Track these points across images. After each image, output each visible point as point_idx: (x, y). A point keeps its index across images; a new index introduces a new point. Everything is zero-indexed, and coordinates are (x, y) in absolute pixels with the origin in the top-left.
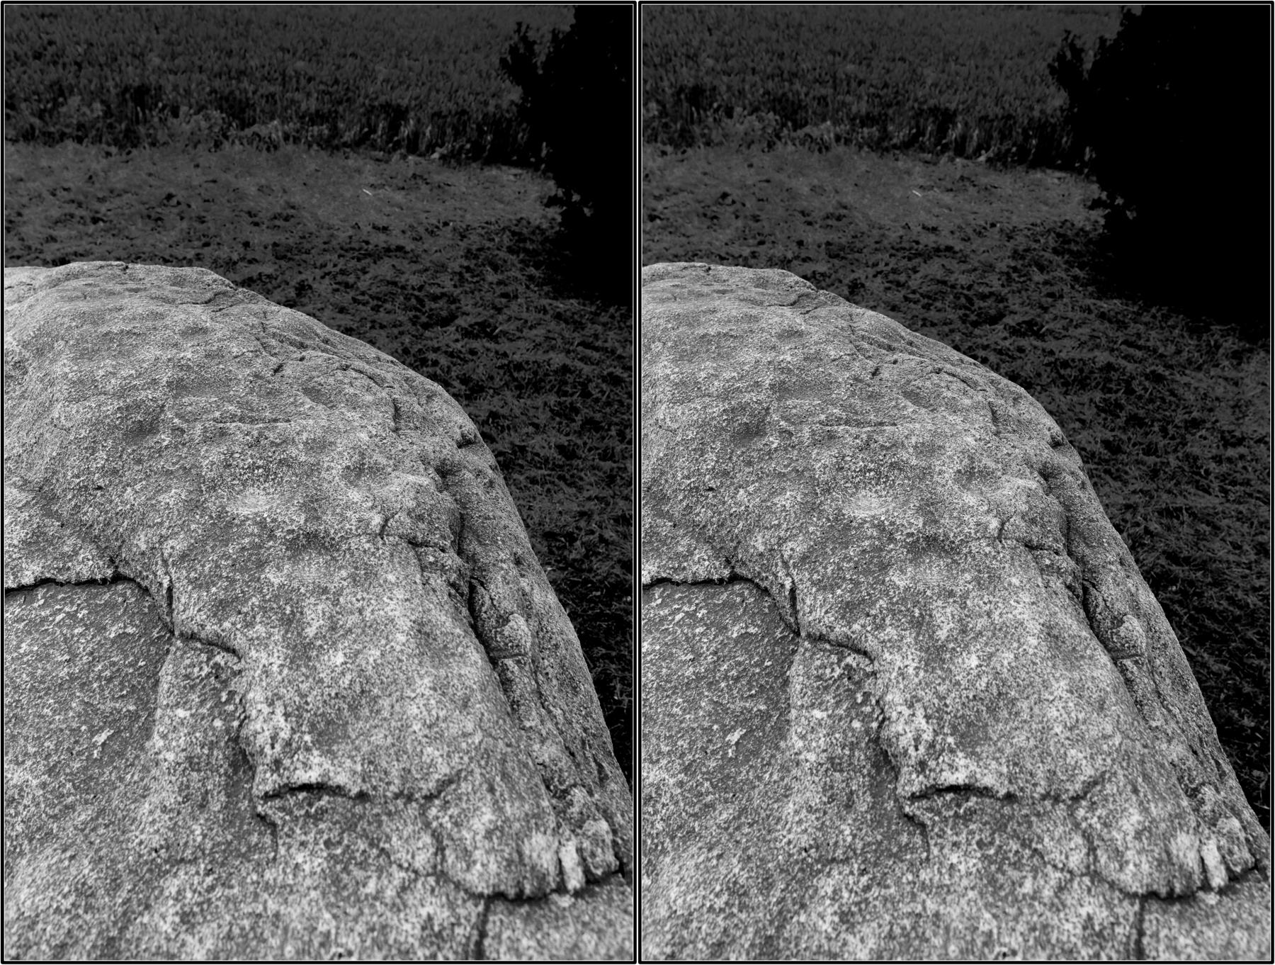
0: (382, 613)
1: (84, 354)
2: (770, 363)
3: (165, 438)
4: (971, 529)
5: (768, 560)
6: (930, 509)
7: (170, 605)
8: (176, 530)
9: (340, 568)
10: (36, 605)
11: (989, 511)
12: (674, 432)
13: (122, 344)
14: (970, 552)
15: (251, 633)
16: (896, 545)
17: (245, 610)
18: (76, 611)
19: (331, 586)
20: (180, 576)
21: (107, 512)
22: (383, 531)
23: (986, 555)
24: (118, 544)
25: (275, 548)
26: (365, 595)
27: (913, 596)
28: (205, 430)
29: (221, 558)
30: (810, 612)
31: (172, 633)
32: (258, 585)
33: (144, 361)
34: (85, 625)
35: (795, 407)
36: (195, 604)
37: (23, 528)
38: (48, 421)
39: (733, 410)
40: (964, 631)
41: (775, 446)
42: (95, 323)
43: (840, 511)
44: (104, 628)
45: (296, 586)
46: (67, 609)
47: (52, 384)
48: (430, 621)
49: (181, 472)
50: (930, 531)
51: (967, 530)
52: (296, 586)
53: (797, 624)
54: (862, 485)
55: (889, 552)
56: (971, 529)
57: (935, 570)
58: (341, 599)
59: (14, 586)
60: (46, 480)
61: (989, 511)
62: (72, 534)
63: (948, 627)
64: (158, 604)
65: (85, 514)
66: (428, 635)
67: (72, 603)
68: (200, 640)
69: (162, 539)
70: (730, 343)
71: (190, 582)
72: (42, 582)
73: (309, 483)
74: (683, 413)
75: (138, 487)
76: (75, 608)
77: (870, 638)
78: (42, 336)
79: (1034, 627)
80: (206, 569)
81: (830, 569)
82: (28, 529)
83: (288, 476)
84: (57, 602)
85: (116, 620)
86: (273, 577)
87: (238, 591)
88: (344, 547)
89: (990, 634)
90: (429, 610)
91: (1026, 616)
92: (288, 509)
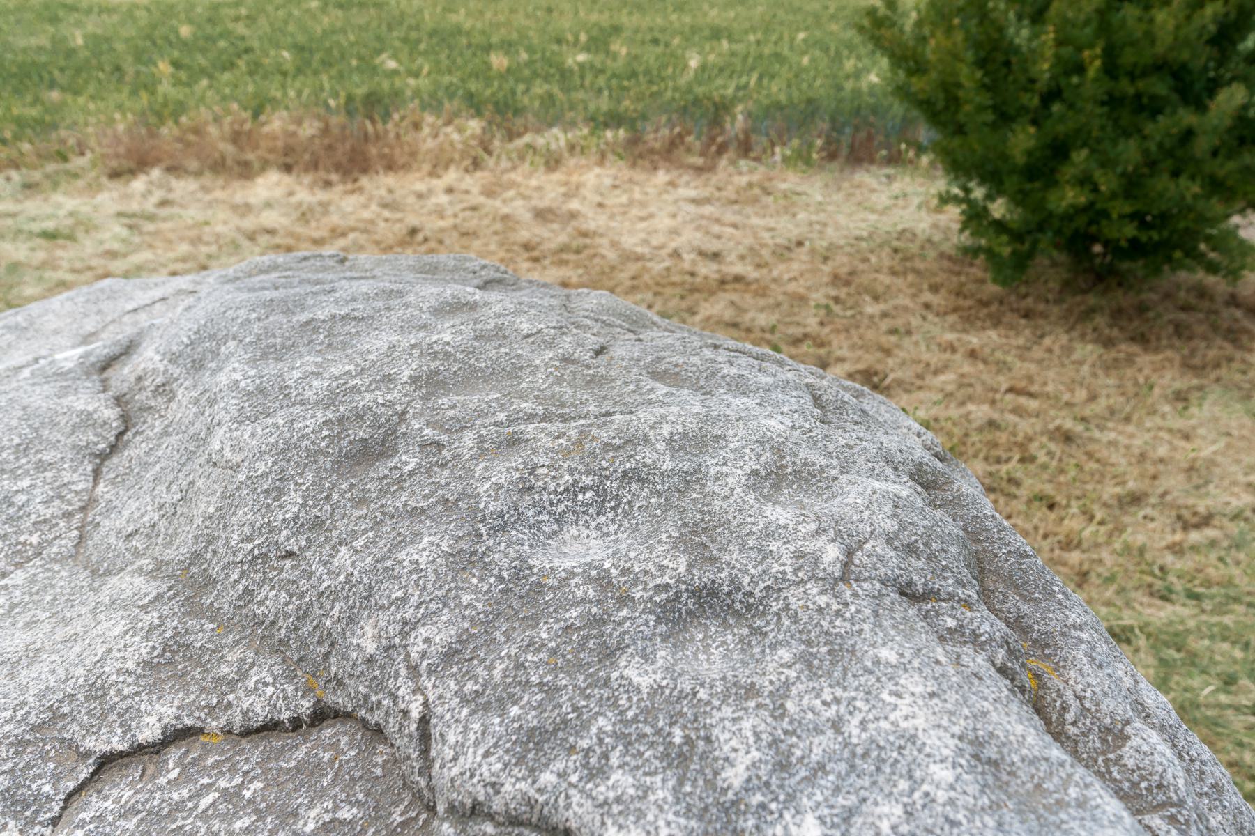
0: (884, 724)
1: (268, 351)
2: (413, 346)
3: (409, 460)
4: (783, 563)
5: (382, 667)
6: (700, 539)
7: (425, 752)
8: (433, 607)
9: (773, 647)
10: (162, 781)
11: (818, 532)
12: (236, 468)
13: (333, 334)
14: (787, 608)
15: (602, 791)
16: (633, 609)
17: (584, 744)
18: (241, 786)
19: (764, 683)
20: (443, 693)
21: (302, 595)
22: (847, 572)
23: (820, 610)
24: (322, 650)
25: (634, 621)
26: (839, 692)
27: (670, 702)
28: (481, 439)
29: (526, 649)
30: (455, 759)
31: (431, 809)
32: (606, 693)
33: (369, 352)
34: (257, 811)
35: (453, 407)
36: (477, 743)
37: (146, 638)
38: (202, 460)
39: (341, 420)
40: (783, 766)
41: (408, 468)
42: (288, 312)
43: (524, 560)
44: (295, 815)
45: (687, 687)
46: (223, 783)
47: (212, 402)
48: (991, 734)
49: (439, 508)
50: (702, 576)
51: (776, 568)
52: (687, 687)
53: (432, 789)
54: (570, 517)
55: (620, 624)
56: (783, 563)
57: (716, 654)
58: (789, 705)
59: (124, 747)
60: (196, 555)
61: (818, 532)
62: (237, 643)
63: (747, 760)
64: (400, 755)
65: (262, 603)
66: (994, 764)
67: (233, 771)
68: (491, 817)
69: (408, 626)
70: (351, 328)
71: (465, 701)
72: (178, 735)
73: (686, 504)
74: (253, 435)
75: (359, 543)
76: (238, 780)
77: (576, 797)
78: (201, 340)
79: (941, 743)
80: (497, 673)
81: (499, 667)
82: (156, 640)
83: (643, 498)
84: (204, 771)
85: (318, 795)
86: (637, 674)
87: (566, 708)
88: (775, 606)
89: (843, 767)
90: (985, 714)
91: (920, 722)
92: (651, 549)
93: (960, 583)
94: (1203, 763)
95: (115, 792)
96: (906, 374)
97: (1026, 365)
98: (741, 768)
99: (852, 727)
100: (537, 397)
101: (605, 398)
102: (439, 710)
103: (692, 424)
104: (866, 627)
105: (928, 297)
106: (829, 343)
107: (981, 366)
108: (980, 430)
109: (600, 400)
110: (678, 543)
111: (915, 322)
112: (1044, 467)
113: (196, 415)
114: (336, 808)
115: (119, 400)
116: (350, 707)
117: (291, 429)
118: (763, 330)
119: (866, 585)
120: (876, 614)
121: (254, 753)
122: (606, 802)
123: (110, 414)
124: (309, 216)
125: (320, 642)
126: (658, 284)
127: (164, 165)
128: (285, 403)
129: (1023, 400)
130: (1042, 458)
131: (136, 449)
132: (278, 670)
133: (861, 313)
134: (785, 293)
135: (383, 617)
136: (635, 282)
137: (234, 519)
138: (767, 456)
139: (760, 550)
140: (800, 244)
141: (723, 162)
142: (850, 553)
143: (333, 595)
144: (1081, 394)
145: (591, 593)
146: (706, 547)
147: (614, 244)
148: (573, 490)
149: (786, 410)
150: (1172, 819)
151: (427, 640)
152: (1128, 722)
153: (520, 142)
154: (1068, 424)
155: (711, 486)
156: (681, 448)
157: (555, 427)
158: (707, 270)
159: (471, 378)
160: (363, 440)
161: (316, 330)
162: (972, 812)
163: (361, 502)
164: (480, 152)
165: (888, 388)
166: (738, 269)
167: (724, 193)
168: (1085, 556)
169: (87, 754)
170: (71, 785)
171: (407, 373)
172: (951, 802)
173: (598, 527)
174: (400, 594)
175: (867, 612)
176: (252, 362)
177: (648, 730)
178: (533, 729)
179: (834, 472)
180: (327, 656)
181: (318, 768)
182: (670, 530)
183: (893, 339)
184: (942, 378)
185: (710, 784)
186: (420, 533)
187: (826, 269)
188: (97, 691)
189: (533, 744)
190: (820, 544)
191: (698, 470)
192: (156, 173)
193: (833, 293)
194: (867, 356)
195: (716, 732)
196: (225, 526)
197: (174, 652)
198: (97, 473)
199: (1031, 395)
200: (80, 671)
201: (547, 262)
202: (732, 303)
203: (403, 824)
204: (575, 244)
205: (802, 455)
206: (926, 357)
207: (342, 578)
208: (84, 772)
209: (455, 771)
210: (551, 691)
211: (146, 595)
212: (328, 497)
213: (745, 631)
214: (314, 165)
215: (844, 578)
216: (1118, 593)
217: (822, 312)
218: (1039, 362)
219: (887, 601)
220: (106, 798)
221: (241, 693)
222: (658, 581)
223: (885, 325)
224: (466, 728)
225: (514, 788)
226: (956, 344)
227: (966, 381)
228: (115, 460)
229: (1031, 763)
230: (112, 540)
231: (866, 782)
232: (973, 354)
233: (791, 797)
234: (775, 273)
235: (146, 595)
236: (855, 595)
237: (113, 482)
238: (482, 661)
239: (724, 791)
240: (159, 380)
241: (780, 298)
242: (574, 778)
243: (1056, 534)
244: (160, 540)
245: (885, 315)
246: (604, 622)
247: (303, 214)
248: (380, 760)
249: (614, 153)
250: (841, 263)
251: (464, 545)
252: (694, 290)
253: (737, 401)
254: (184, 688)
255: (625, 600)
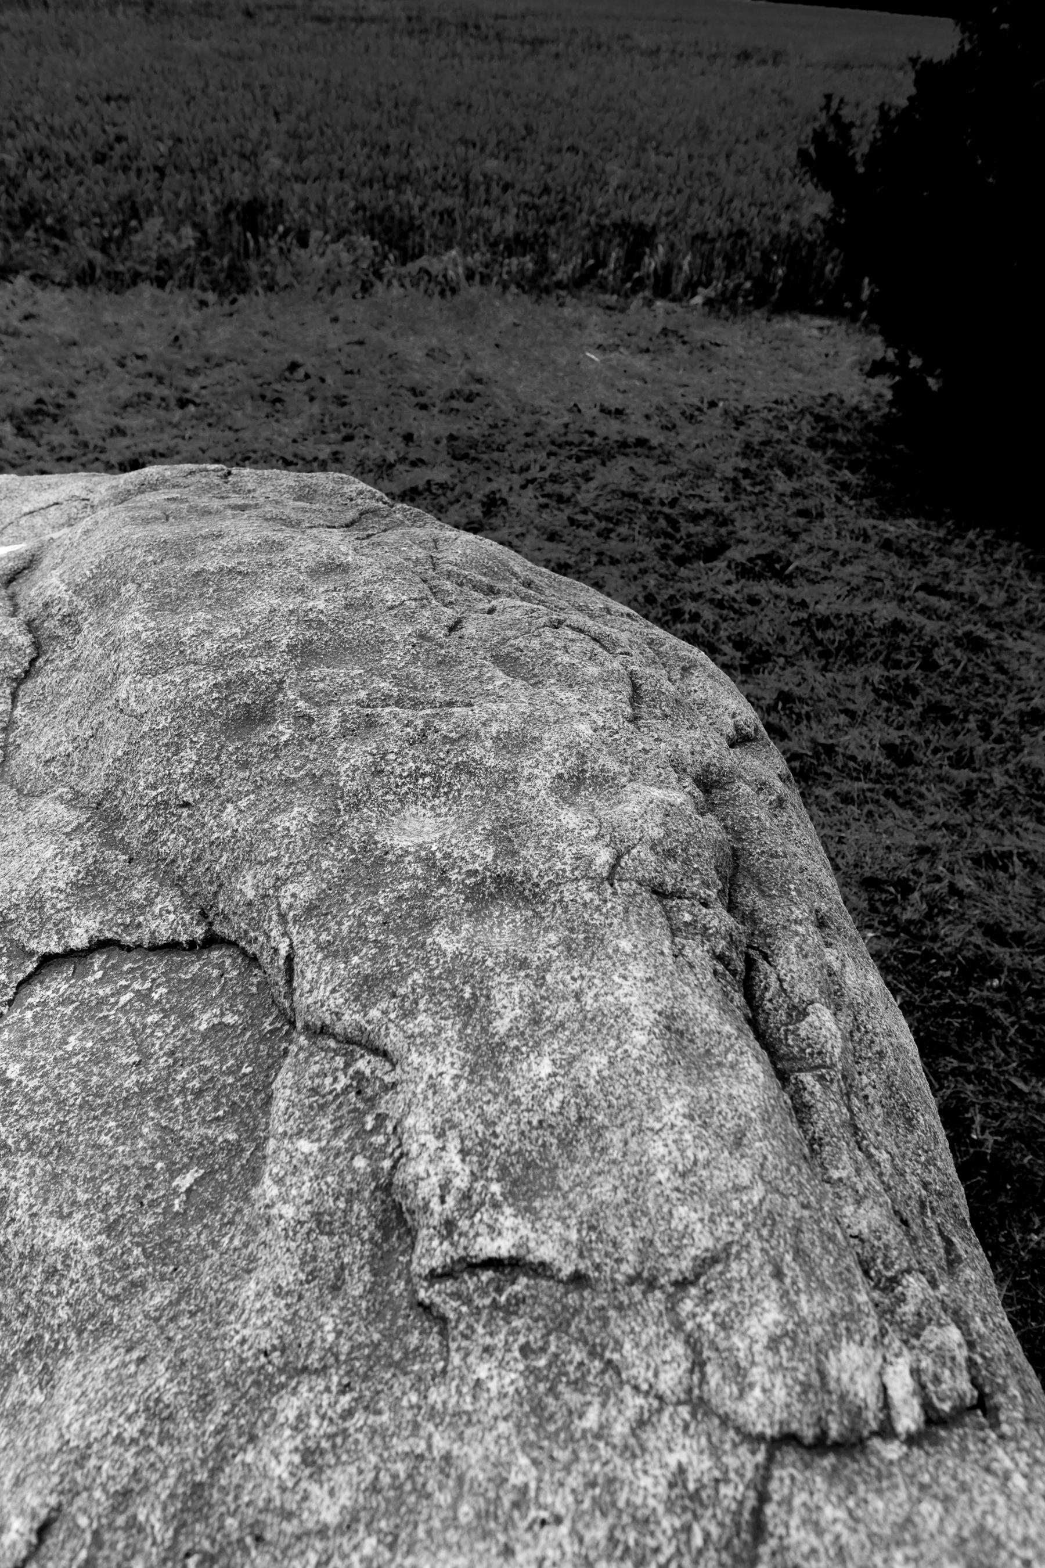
0: (610, 998)
1: (165, 603)
3: (285, 731)
4: (565, 864)
5: (259, 911)
7: (289, 981)
8: (299, 868)
9: (546, 930)
10: (90, 979)
11: (597, 838)
12: (140, 718)
13: (218, 588)
14: (561, 900)
15: (411, 1027)
16: (449, 888)
17: (402, 991)
19: (533, 957)
21: (196, 841)
23: (585, 905)
24: (213, 888)
27: (464, 967)
28: (344, 718)
29: (367, 912)
30: (310, 991)
31: (292, 1024)
33: (253, 614)
34: (163, 1010)
35: (323, 680)
37: (72, 863)
38: (110, 703)
39: (229, 684)
40: (536, 1022)
41: (284, 738)
42: (181, 557)
43: (371, 836)
45: (480, 956)
46: (136, 986)
47: (117, 649)
48: (684, 1012)
49: (308, 781)
50: (503, 867)
51: (559, 866)
52: (480, 956)
53: (293, 1010)
55: (438, 899)
56: (565, 864)
57: (507, 928)
59: (59, 950)
60: (108, 792)
61: (597, 838)
62: (144, 874)
63: (512, 1015)
65: (164, 843)
67: (144, 977)
68: (334, 1036)
69: (280, 882)
71: (320, 948)
72: (100, 945)
74: (154, 690)
76: (148, 985)
77: (393, 1030)
79: (646, 1017)
84: (122, 975)
85: (209, 1003)
86: (446, 942)
88: (554, 897)
91: (634, 1000)
92: (468, 838)
93: (706, 884)
94: (876, 1034)
95: (54, 985)
96: (812, 562)
97: (945, 560)
98: (506, 1021)
99: (588, 999)
100: (394, 676)
101: (451, 683)
102: (301, 952)
103: (517, 723)
104: (615, 921)
105: (846, 475)
106: (733, 522)
107: (894, 559)
108: (882, 631)
109: (448, 684)
110: (492, 835)
111: (829, 503)
112: (947, 675)
113: (102, 657)
114: (222, 1015)
115: (31, 627)
116: (233, 938)
117: (187, 689)
118: (662, 503)
119: (625, 885)
120: (626, 911)
121: (158, 967)
122: (412, 1036)
123: (23, 640)
124: (182, 340)
125: (211, 883)
126: (553, 443)
127: (28, 273)
128: (181, 660)
129: (934, 600)
130: (945, 664)
131: (46, 679)
132: (178, 901)
133: (771, 489)
134: (689, 461)
135: (262, 871)
136: (529, 440)
137: (140, 766)
138: (573, 761)
139: (550, 849)
140: (713, 404)
141: (637, 302)
142: (618, 857)
143: (221, 845)
144: (1000, 596)
145: (419, 871)
146: (511, 841)
147: (510, 392)
148: (416, 775)
149: (601, 708)
150: (821, 1078)
151: (293, 895)
152: (812, 1003)
153: (412, 267)
154: (981, 630)
155: (523, 786)
156: (505, 746)
157: (405, 714)
158: (610, 429)
159: (340, 651)
160: (246, 705)
161: (205, 583)
162: (653, 1066)
163: (245, 765)
164: (371, 277)
165: (790, 576)
166: (644, 432)
167: (635, 339)
168: (974, 775)
169: (32, 954)
170: (21, 976)
171: (285, 641)
172: (641, 1058)
173: (433, 808)
174: (274, 854)
175: (620, 908)
176: (150, 611)
177: (448, 986)
178: (367, 977)
179: (624, 780)
180: (216, 894)
181: (206, 982)
182: (486, 823)
183: (802, 521)
184: (849, 569)
185: (484, 1030)
186: (291, 803)
187: (739, 435)
188: (36, 903)
189: (366, 988)
190: (596, 848)
191: (515, 770)
192: (21, 281)
193: (743, 465)
194: (773, 540)
195: (494, 992)
196: (132, 771)
197: (94, 877)
198: (14, 696)
199: (947, 596)
200: (21, 886)
201: (435, 411)
202: (632, 469)
203: (271, 1032)
204: (466, 390)
205: (601, 762)
206: (834, 544)
207: (229, 832)
208: (30, 967)
209: (310, 1000)
210: (383, 948)
211: (69, 823)
212: (217, 758)
213: (530, 913)
214: (188, 282)
215: (610, 879)
216: (1003, 816)
217: (729, 487)
218: (959, 558)
219: (639, 899)
220: (48, 988)
221: (149, 916)
222: (471, 867)
223: (795, 505)
224: (320, 969)
225: (351, 1018)
226: (870, 532)
227: (875, 574)
228: (29, 685)
229: (708, 1034)
230: (33, 764)
231: (589, 1039)
232: (887, 545)
233: (537, 1044)
234: (681, 439)
235: (69, 823)
236: (615, 894)
237: (28, 706)
238: (334, 917)
239: (493, 1035)
240: (65, 610)
241: (685, 467)
242: (392, 1016)
243: (947, 750)
244: (74, 769)
245: (796, 494)
246: (427, 896)
247: (177, 339)
248: (255, 981)
249: (519, 286)
250: (757, 429)
251: (325, 818)
252: (593, 452)
253: (562, 695)
254: (104, 906)
255: (443, 880)
